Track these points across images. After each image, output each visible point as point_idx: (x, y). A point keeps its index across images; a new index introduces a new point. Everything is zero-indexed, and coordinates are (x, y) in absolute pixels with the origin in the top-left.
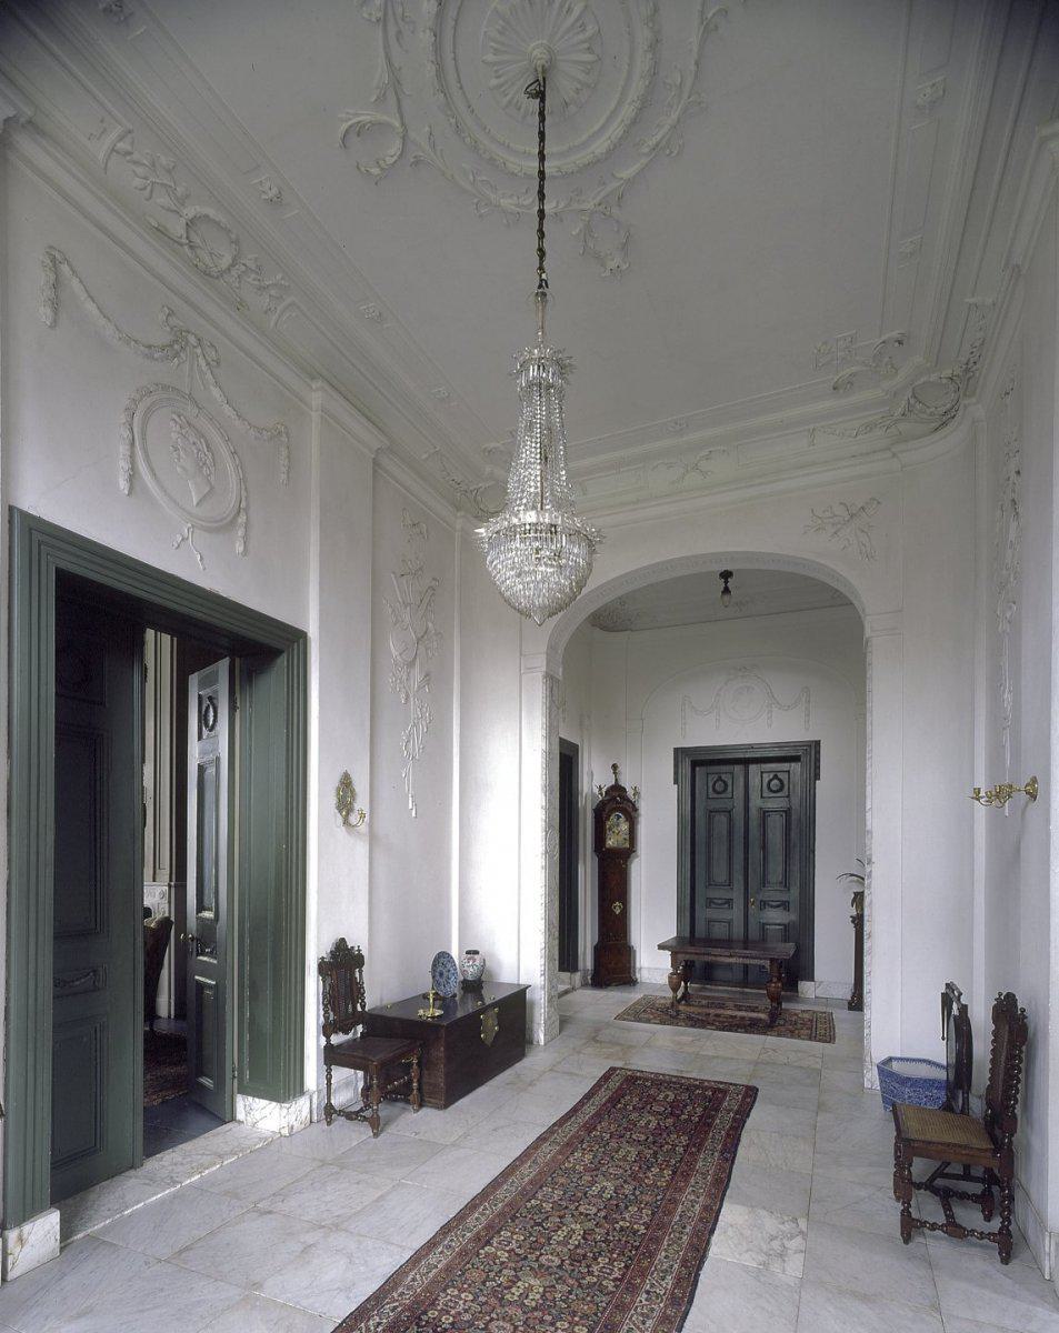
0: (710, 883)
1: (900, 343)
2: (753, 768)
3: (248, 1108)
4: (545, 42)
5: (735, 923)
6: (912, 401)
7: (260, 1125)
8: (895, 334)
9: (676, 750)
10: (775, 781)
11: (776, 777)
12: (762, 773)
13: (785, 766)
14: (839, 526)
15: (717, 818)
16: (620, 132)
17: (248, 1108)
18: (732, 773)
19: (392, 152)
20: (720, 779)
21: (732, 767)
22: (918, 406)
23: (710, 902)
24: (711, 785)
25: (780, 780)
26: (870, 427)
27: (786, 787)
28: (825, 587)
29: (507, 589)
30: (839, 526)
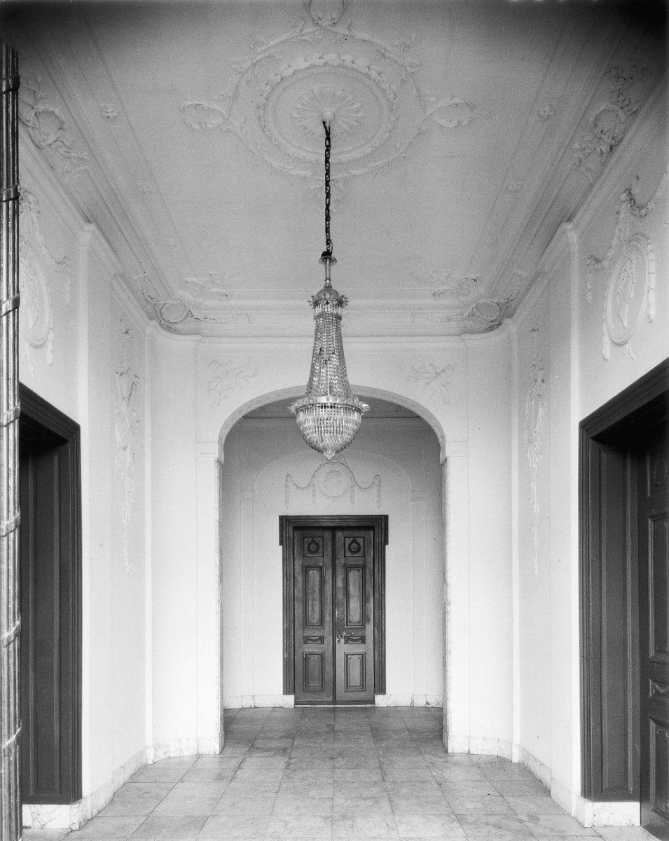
0: (306, 623)
1: (475, 280)
2: (339, 535)
3: (35, 815)
4: (333, 110)
5: (327, 654)
6: (475, 310)
7: (48, 826)
8: (474, 277)
9: (282, 518)
10: (354, 545)
11: (355, 541)
12: (345, 538)
13: (362, 533)
14: (429, 380)
15: (311, 572)
16: (359, 155)
17: (35, 815)
18: (323, 538)
19: (213, 122)
20: (313, 541)
21: (363, 532)
22: (478, 314)
23: (307, 640)
24: (347, 545)
25: (358, 544)
26: (449, 320)
27: (362, 549)
28: (399, 408)
29: (306, 429)
30: (429, 380)
